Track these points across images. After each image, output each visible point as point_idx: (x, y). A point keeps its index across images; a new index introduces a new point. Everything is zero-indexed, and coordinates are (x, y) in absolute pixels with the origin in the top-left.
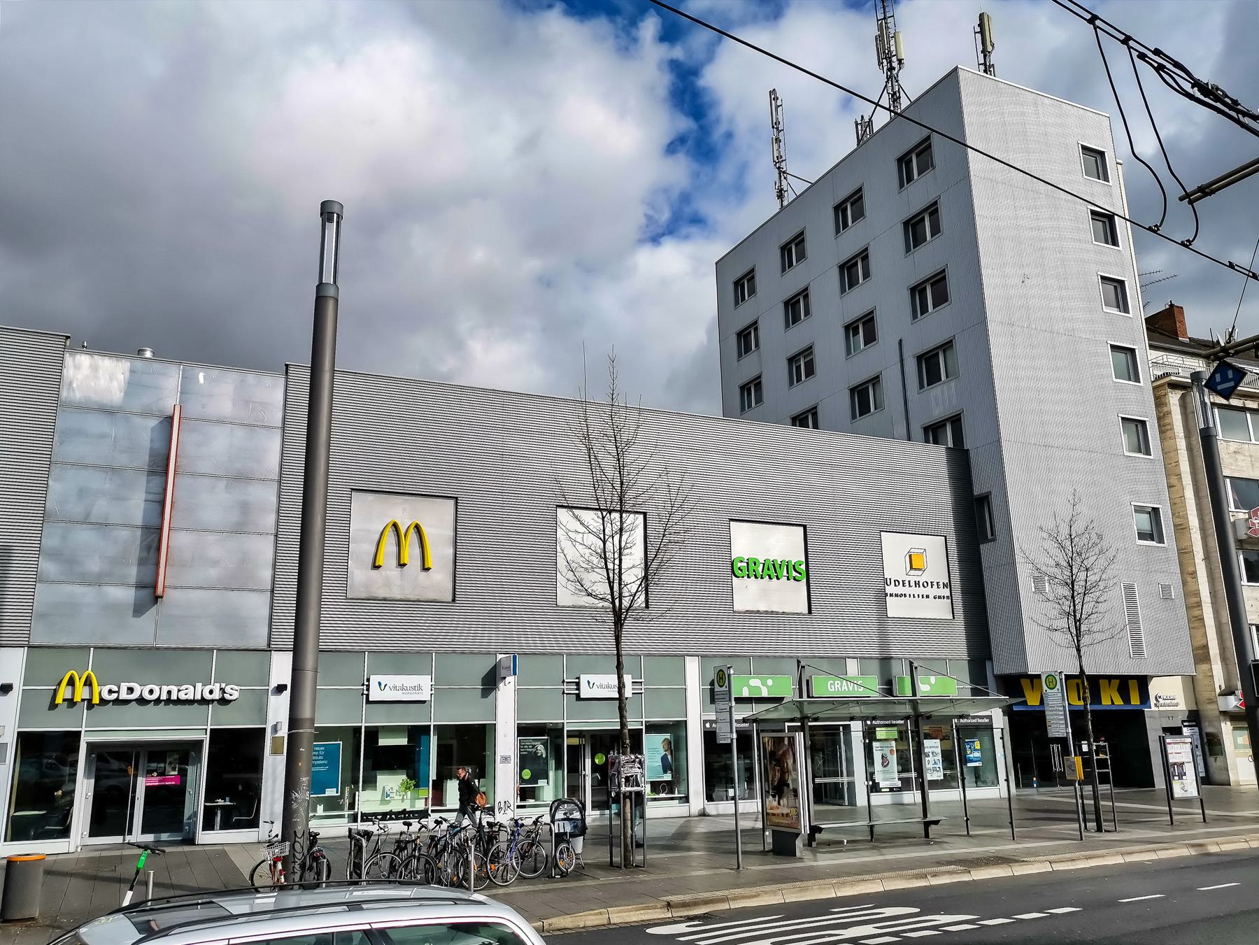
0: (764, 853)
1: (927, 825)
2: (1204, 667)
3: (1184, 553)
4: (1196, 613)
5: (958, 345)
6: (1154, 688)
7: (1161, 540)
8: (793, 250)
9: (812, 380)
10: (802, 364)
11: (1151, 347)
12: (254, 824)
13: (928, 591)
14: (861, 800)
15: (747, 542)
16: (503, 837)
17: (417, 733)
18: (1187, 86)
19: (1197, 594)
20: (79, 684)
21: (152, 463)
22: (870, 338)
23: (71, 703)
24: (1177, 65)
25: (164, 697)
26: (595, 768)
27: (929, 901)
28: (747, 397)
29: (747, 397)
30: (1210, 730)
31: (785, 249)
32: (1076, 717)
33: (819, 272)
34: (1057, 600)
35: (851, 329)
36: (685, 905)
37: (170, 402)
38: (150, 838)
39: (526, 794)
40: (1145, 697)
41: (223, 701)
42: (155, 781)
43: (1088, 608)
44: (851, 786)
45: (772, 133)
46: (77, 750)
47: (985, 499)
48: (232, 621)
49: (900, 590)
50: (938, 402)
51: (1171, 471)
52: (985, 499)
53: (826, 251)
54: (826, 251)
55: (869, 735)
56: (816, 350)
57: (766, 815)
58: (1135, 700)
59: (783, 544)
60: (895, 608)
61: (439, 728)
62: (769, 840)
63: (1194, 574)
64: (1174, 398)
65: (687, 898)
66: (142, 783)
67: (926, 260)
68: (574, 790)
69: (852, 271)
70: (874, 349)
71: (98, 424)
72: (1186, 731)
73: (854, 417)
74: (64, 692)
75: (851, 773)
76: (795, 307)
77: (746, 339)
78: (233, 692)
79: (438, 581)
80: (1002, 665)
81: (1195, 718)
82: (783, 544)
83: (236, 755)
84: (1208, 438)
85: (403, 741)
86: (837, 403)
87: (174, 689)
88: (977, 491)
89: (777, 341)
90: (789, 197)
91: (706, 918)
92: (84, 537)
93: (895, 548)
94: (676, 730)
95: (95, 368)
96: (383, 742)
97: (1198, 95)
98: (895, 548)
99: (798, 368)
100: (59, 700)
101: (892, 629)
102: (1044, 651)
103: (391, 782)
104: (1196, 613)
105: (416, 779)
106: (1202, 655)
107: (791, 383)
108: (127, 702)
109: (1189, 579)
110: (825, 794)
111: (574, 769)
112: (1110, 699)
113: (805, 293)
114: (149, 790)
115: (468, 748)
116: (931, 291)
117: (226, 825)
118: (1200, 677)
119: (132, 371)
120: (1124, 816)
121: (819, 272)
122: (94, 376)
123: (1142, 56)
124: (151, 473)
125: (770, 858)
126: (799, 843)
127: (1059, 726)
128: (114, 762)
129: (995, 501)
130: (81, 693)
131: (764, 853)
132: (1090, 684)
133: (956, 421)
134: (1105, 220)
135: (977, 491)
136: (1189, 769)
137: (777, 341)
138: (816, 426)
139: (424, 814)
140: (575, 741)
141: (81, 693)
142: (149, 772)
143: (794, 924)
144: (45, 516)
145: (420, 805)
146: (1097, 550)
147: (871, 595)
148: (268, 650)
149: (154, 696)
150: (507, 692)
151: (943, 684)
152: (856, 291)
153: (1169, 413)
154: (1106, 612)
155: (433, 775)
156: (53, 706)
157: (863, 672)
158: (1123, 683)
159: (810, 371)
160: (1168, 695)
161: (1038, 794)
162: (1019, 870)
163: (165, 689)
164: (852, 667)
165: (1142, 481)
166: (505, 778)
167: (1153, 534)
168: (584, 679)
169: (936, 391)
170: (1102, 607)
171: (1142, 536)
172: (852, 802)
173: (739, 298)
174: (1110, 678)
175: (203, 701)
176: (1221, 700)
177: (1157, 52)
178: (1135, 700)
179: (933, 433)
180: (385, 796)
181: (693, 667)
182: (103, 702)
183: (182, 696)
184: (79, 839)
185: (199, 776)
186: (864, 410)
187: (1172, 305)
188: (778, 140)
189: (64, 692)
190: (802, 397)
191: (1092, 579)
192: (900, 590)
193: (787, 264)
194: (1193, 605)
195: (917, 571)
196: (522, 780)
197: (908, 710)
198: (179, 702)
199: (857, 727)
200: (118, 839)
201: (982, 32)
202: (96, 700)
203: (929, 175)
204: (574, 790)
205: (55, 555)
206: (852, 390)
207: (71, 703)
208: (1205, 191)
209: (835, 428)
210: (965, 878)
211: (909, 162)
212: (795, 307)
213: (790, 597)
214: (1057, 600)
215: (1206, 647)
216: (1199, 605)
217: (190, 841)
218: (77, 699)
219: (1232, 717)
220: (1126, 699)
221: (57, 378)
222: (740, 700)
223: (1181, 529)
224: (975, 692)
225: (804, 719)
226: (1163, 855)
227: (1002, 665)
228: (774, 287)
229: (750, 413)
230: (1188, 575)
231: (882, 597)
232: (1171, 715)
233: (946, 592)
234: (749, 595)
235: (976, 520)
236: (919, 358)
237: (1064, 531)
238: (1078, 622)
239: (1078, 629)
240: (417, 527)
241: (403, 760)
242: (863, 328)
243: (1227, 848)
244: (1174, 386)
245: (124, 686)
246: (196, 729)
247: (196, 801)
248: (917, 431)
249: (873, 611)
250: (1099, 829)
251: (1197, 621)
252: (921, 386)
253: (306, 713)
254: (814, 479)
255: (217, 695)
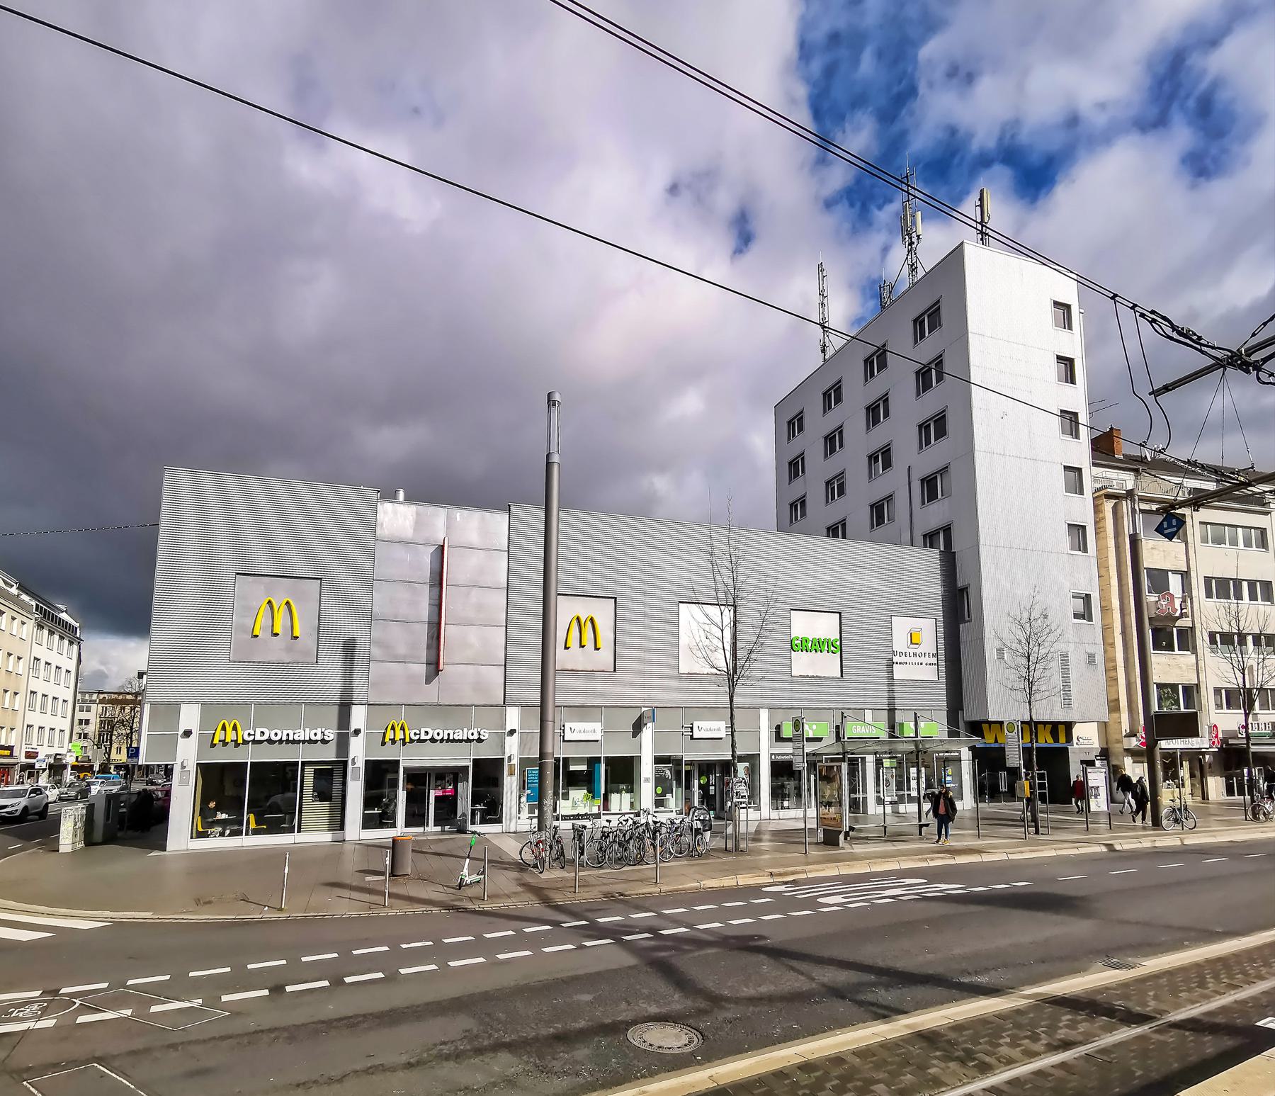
0: (817, 844)
1: (921, 826)
2: (1115, 715)
3: (1107, 628)
4: (1112, 674)
5: (952, 469)
6: (1076, 731)
7: (1090, 619)
8: (833, 395)
9: (843, 499)
10: (836, 487)
11: (1094, 465)
12: (499, 821)
13: (923, 660)
14: (871, 811)
15: (806, 626)
16: (664, 830)
17: (593, 762)
18: (1169, 331)
19: (1114, 660)
20: (229, 729)
21: (432, 578)
22: (887, 465)
23: (224, 743)
24: (1164, 318)
25: (284, 738)
26: (700, 787)
27: (933, 875)
28: (795, 513)
29: (795, 513)
30: (1115, 762)
31: (826, 395)
32: (1027, 751)
33: (851, 413)
34: (1017, 667)
35: (873, 458)
36: (780, 875)
37: (440, 536)
38: (439, 829)
39: (659, 803)
40: (1069, 738)
41: (480, 740)
42: (440, 793)
43: (1037, 674)
44: (865, 799)
45: (817, 299)
46: (397, 772)
47: (964, 590)
48: (479, 686)
49: (903, 659)
50: (933, 516)
51: (1102, 565)
52: (964, 590)
53: (857, 395)
54: (857, 395)
55: (879, 763)
56: (847, 475)
57: (820, 819)
58: (1062, 739)
59: (826, 627)
60: (899, 672)
61: (606, 758)
62: (821, 835)
63: (1112, 645)
64: (1108, 505)
65: (781, 870)
66: (433, 794)
67: (929, 405)
68: (688, 799)
69: (876, 412)
70: (890, 473)
71: (399, 552)
72: (1098, 763)
73: (872, 527)
74: (219, 735)
75: (865, 791)
76: (832, 442)
77: (795, 467)
78: (485, 736)
79: (604, 658)
80: (970, 714)
81: (1105, 754)
82: (826, 627)
83: (487, 775)
84: (1134, 541)
85: (584, 768)
86: (860, 517)
87: (291, 733)
88: (960, 584)
89: (819, 468)
90: (830, 352)
91: (794, 882)
92: (395, 629)
93: (901, 627)
94: (753, 759)
95: (395, 512)
96: (572, 768)
97: (1175, 335)
98: (901, 627)
99: (833, 489)
100: (216, 741)
101: (897, 688)
102: (1002, 702)
103: (578, 794)
104: (1112, 674)
105: (592, 792)
106: (1114, 707)
107: (827, 501)
108: (425, 741)
109: (1108, 648)
110: (855, 805)
111: (688, 787)
112: (1045, 740)
113: (840, 430)
114: (437, 798)
115: (622, 772)
116: (934, 428)
117: (483, 821)
118: (1111, 723)
119: (418, 514)
120: (1054, 825)
121: (851, 413)
122: (397, 517)
123: (1142, 315)
124: (431, 586)
125: (822, 847)
126: (842, 837)
127: (1014, 759)
128: (418, 778)
129: (972, 591)
130: (230, 736)
131: (817, 844)
132: (1031, 726)
133: (947, 530)
134: (1067, 364)
135: (960, 584)
136: (1103, 792)
137: (819, 468)
138: (844, 537)
139: (598, 816)
140: (688, 768)
141: (230, 736)
142: (436, 788)
143: (852, 887)
144: (373, 618)
145: (595, 810)
146: (1047, 630)
147: (884, 665)
148: (505, 705)
149: (278, 738)
150: (647, 734)
151: (934, 728)
152: (878, 428)
153: (1104, 518)
154: (1050, 678)
155: (603, 791)
156: (383, 743)
157: (875, 719)
158: (1054, 727)
159: (842, 492)
160: (1086, 737)
161: (988, 807)
162: (986, 858)
163: (285, 732)
164: (868, 715)
165: (1082, 573)
166: (647, 791)
167: (1086, 615)
168: (696, 724)
169: (934, 506)
170: (1047, 673)
171: (1076, 616)
172: (865, 812)
173: (791, 435)
174: (1045, 723)
175: (468, 741)
176: (1125, 740)
177: (1153, 312)
178: (1062, 739)
179: (930, 539)
180: (574, 805)
181: (764, 714)
182: (412, 741)
183: (297, 738)
184: (400, 829)
185: (466, 789)
186: (880, 521)
187: (1111, 429)
188: (823, 304)
189: (219, 735)
190: (834, 512)
191: (1043, 651)
192: (903, 659)
193: (827, 407)
194: (1110, 669)
195: (916, 642)
196: (657, 794)
197: (912, 747)
198: (454, 741)
199: (870, 759)
200: (421, 829)
201: (981, 206)
202: (240, 741)
203: (936, 333)
204: (688, 799)
205: (381, 644)
206: (872, 506)
207: (393, 741)
208: (1166, 388)
209: (859, 538)
210: (952, 862)
211: (922, 323)
212: (832, 442)
213: (828, 665)
214: (1017, 667)
215: (1118, 700)
216: (1115, 668)
217: (462, 830)
218: (228, 740)
219: (1130, 752)
220: (1056, 740)
221: (372, 520)
222: (809, 740)
223: (1105, 609)
224: (951, 734)
225: (844, 753)
226: (1082, 851)
227: (970, 714)
228: (818, 424)
229: (795, 525)
230: (1108, 644)
231: (891, 664)
232: (1088, 751)
233: (934, 660)
234: (803, 664)
235: (958, 605)
236: (922, 481)
237: (1025, 615)
238: (1031, 684)
239: (1030, 689)
240: (592, 620)
241: (584, 780)
242: (883, 457)
243: (1126, 847)
244: (1109, 496)
245: (258, 731)
246: (463, 758)
247: (465, 805)
248: (919, 539)
249: (883, 675)
250: (1037, 832)
251: (1112, 681)
252: (923, 503)
253: (549, 750)
254: (849, 578)
255: (476, 737)
